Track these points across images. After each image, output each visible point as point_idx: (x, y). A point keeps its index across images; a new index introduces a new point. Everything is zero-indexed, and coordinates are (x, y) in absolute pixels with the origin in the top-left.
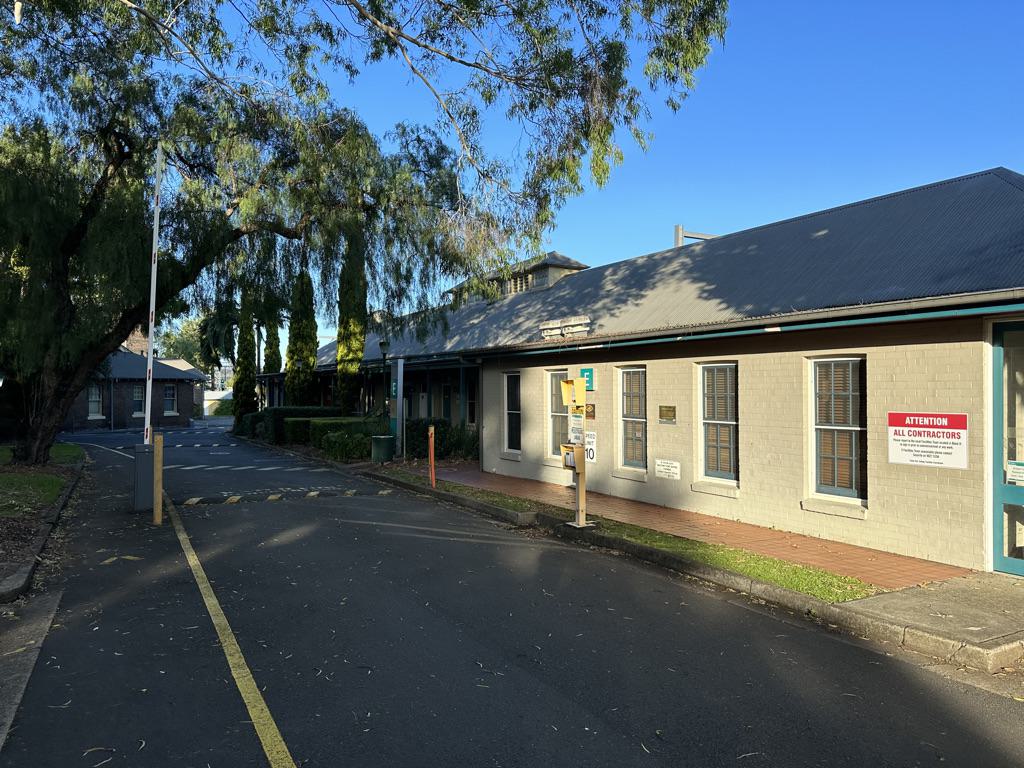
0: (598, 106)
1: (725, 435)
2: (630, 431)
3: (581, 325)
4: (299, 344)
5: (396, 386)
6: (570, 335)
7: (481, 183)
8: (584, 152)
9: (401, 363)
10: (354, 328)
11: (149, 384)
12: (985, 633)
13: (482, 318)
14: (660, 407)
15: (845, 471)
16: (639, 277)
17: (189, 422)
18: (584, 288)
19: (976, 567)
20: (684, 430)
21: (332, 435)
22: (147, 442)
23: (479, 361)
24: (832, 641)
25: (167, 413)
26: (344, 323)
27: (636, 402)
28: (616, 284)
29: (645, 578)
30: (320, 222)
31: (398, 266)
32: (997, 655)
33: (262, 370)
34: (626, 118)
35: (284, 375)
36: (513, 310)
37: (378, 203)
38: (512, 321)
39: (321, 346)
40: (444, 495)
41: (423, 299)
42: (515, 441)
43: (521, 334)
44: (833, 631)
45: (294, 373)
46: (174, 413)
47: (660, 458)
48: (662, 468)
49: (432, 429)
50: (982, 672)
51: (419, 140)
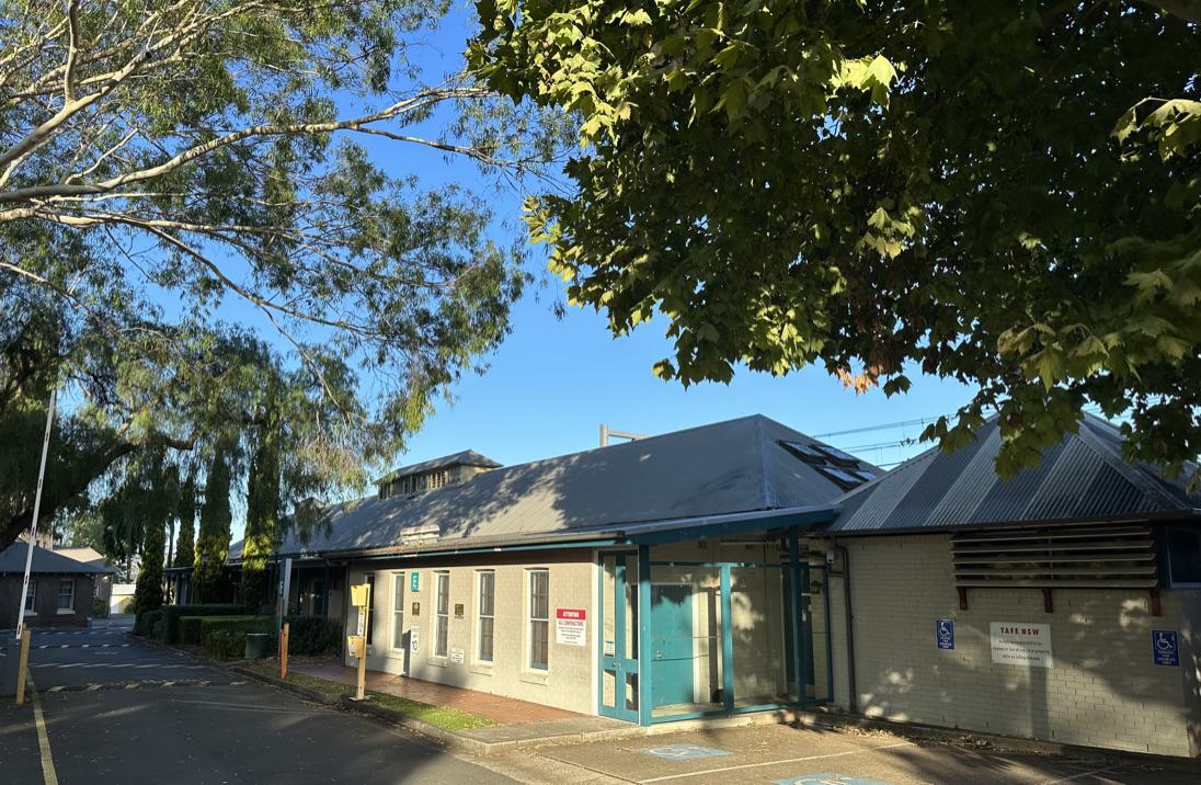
4: (210, 537)
11: (27, 573)
16: (526, 479)
17: (86, 621)
21: (216, 634)
22: (18, 637)
23: (345, 563)
25: (61, 612)
46: (69, 611)
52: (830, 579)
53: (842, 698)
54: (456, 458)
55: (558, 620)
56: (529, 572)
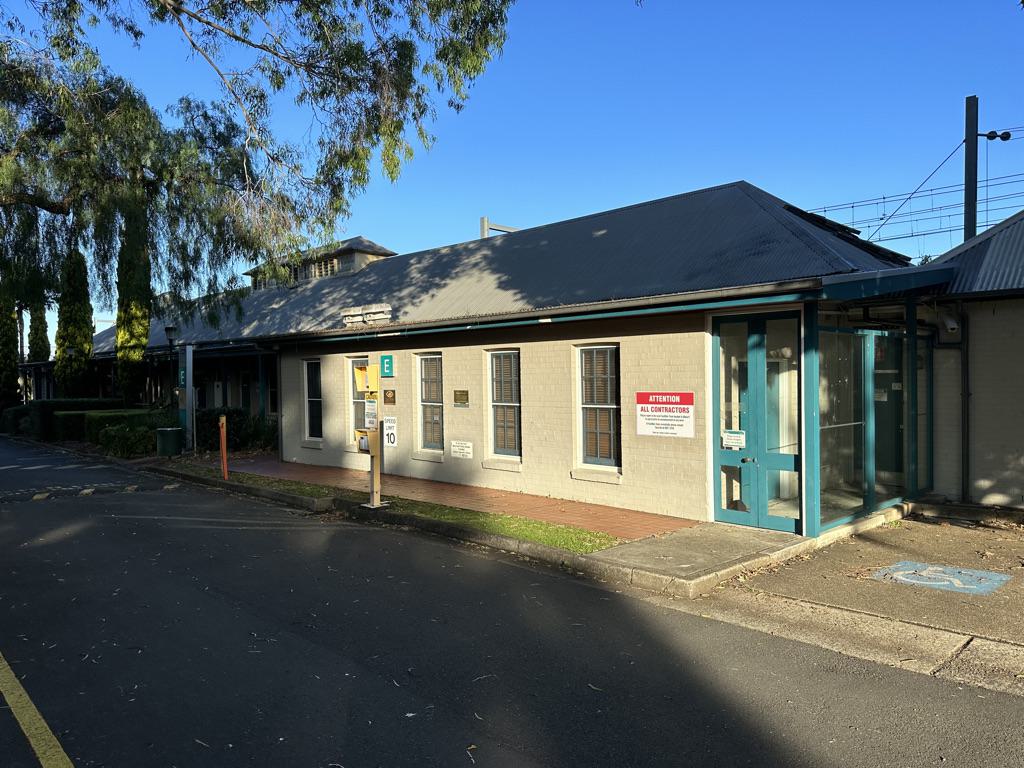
0: (388, 101)
1: (511, 414)
2: (429, 415)
3: (383, 312)
5: (185, 375)
6: (371, 323)
7: (271, 166)
8: (374, 144)
9: (190, 350)
10: (135, 311)
12: (693, 568)
13: (282, 303)
14: (455, 392)
15: (604, 444)
16: (443, 266)
18: (391, 275)
19: (702, 519)
20: (475, 412)
21: (112, 429)
24: (574, 585)
26: (123, 305)
27: (434, 387)
28: (421, 272)
29: (428, 553)
30: (92, 197)
31: (184, 247)
32: (696, 585)
33: (27, 358)
34: (414, 114)
35: (54, 363)
36: (317, 295)
37: (161, 179)
38: (316, 307)
39: (98, 331)
40: (237, 486)
41: (212, 284)
42: (316, 429)
43: (324, 321)
44: (579, 578)
45: (65, 361)
47: (455, 439)
48: (456, 449)
49: (223, 419)
50: (686, 599)
51: (206, 116)
52: (935, 350)
53: (947, 483)
54: (345, 245)
55: (639, 406)
56: (578, 350)
